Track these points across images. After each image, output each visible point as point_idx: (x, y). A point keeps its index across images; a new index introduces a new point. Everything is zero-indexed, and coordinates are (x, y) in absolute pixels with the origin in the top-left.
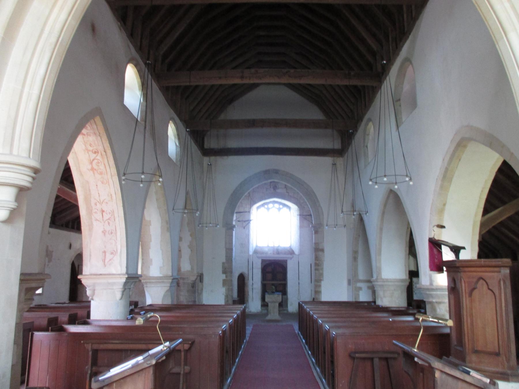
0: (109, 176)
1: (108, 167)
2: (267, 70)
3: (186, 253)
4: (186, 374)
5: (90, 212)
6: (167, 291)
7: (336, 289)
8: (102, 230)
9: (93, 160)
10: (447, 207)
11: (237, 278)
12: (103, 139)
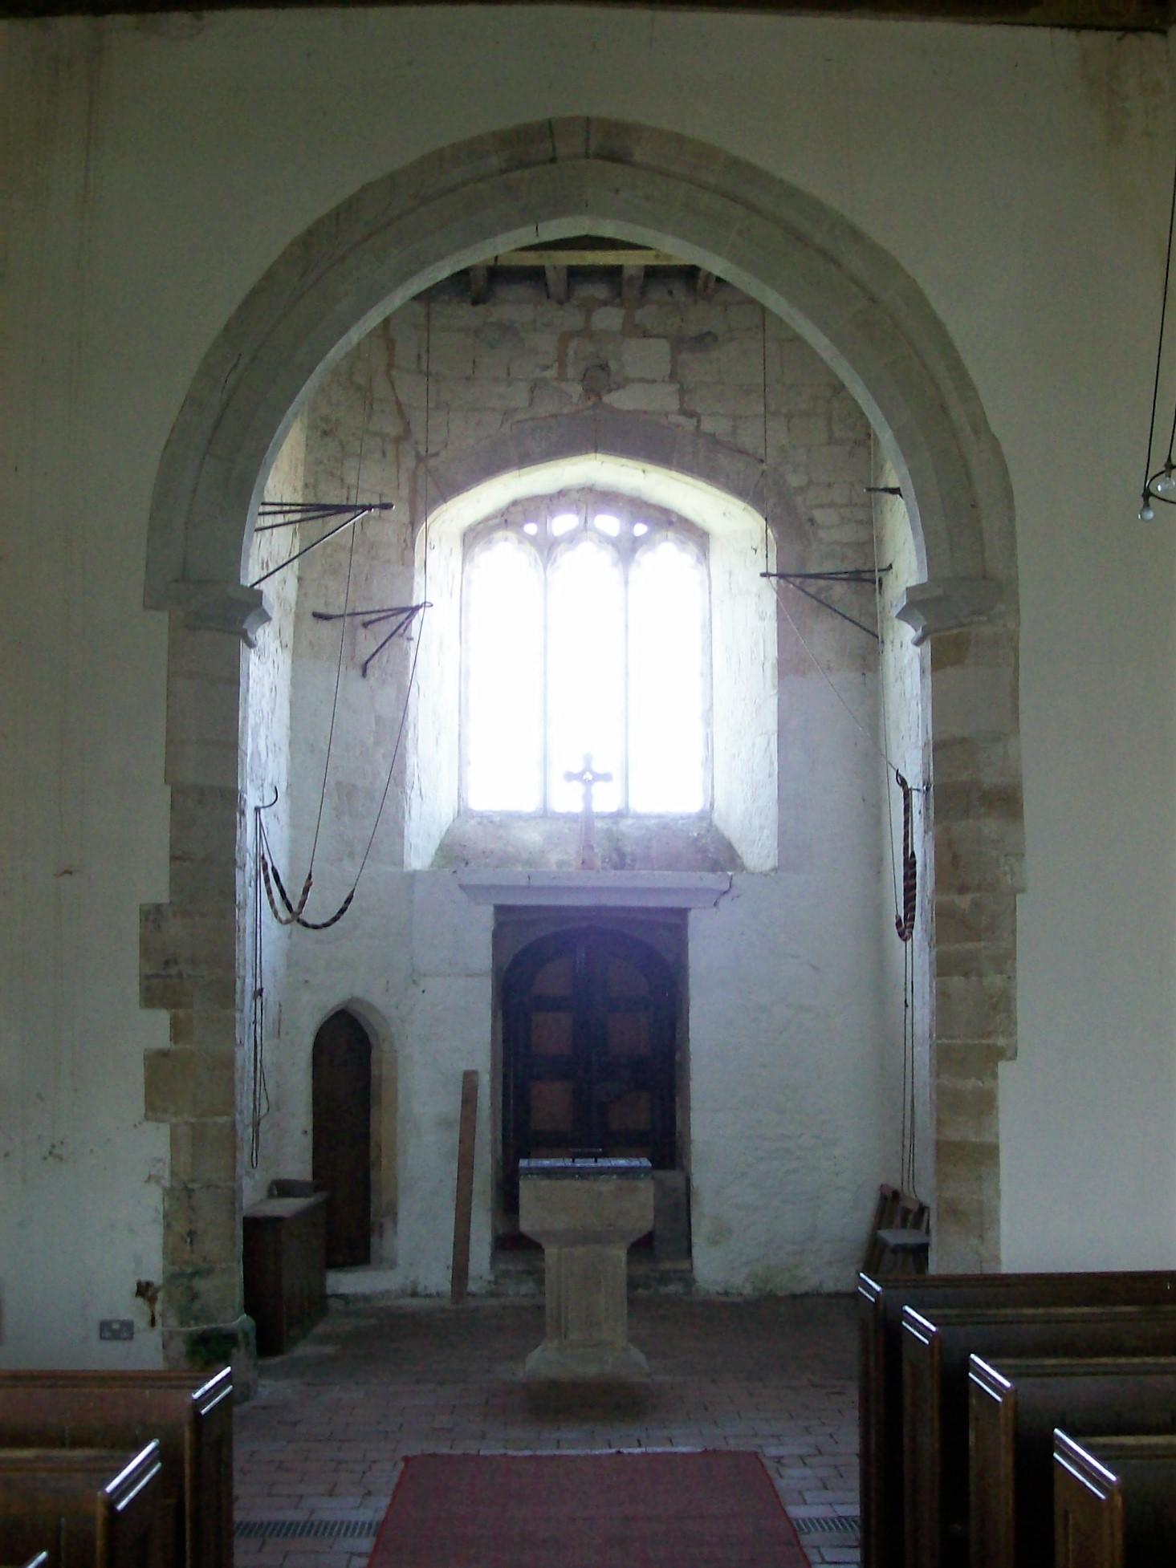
11: (308, 1041)
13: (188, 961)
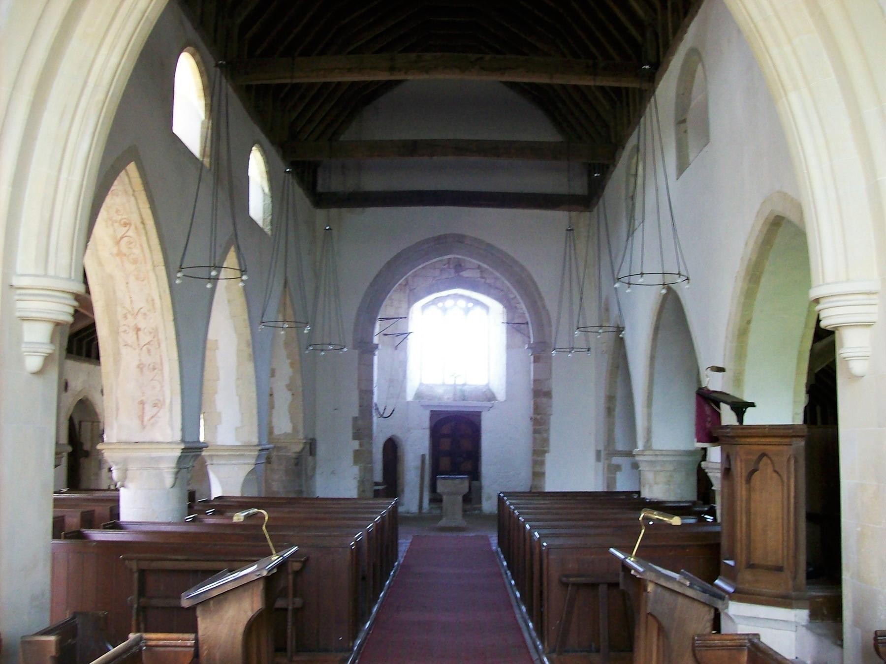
0: (149, 267)
1: (147, 250)
2: (438, 54)
3: (283, 399)
4: (297, 611)
5: (115, 332)
6: (251, 472)
7: (575, 471)
8: (137, 363)
9: (122, 238)
10: (753, 326)
12: (139, 201)
13: (362, 431)
